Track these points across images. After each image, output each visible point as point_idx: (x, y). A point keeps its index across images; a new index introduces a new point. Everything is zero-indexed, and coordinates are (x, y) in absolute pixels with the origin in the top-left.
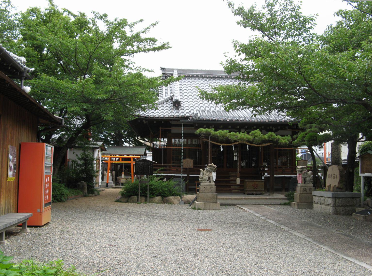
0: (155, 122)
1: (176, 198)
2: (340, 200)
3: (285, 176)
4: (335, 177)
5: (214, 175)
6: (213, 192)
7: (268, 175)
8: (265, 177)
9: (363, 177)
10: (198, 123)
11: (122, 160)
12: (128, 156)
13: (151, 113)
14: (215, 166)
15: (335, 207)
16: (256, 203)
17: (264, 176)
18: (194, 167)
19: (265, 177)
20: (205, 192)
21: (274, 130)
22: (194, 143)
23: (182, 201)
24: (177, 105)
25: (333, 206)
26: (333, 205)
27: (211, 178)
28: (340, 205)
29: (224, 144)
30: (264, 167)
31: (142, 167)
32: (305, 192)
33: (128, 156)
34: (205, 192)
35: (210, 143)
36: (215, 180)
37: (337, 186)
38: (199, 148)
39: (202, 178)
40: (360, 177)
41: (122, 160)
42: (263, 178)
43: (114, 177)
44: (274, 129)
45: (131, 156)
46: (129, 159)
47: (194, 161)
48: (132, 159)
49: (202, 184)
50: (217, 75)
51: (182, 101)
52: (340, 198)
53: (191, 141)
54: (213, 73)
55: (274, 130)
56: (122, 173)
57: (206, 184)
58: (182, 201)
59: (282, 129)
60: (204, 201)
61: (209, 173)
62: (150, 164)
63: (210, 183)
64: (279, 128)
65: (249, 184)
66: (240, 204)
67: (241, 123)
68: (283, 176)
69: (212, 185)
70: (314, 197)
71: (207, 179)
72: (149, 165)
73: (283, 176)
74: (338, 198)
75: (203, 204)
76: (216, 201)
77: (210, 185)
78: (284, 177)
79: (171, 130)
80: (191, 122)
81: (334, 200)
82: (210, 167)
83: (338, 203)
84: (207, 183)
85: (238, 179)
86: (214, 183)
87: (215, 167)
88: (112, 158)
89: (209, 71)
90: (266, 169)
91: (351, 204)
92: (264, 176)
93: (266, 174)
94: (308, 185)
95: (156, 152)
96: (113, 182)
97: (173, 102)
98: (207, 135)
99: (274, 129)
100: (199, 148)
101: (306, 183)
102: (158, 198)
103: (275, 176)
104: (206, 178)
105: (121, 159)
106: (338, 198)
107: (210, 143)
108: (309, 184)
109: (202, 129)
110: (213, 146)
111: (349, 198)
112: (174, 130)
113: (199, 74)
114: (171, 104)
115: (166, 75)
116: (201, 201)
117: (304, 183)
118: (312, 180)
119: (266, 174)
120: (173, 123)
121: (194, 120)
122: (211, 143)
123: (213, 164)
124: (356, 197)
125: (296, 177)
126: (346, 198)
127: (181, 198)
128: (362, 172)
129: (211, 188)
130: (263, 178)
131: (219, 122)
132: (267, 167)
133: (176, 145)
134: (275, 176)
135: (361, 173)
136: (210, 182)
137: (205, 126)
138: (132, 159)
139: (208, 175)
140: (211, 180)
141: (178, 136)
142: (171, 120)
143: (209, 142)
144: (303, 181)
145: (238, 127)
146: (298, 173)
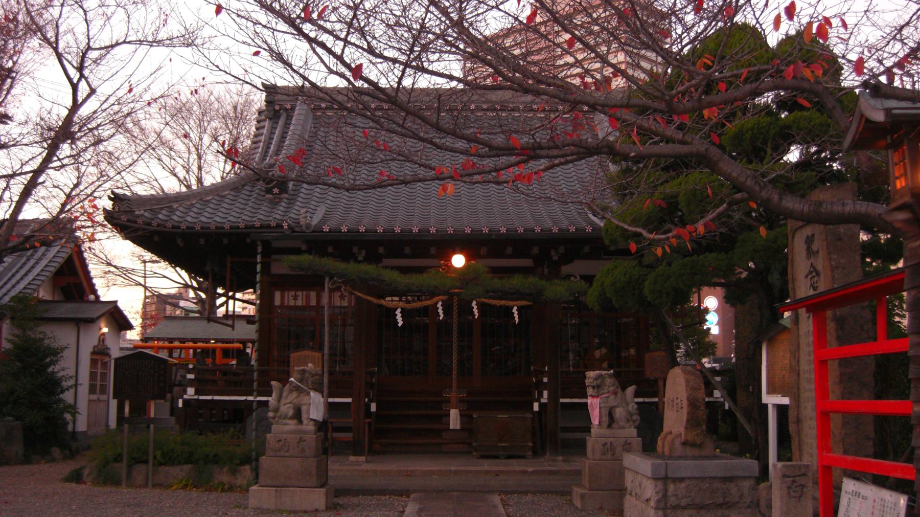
0: (225, 241)
2: (683, 485)
8: (186, 402)
9: (774, 405)
15: (665, 509)
17: (185, 397)
19: (186, 402)
22: (292, 303)
25: (657, 509)
26: (658, 501)
27: (304, 408)
28: (683, 503)
30: (540, 373)
32: (609, 456)
34: (282, 453)
39: (276, 410)
40: (766, 406)
52: (682, 480)
53: (282, 297)
57: (287, 428)
61: (295, 394)
63: (299, 427)
69: (305, 432)
70: (627, 472)
71: (291, 413)
73: (574, 400)
74: (675, 480)
78: (212, 400)
81: (660, 485)
83: (676, 495)
84: (292, 425)
85: (454, 414)
86: (311, 427)
90: (191, 376)
91: (720, 500)
92: (185, 397)
93: (191, 391)
94: (620, 432)
96: (173, 419)
101: (614, 425)
102: (180, 472)
103: (562, 400)
104: (287, 409)
106: (675, 480)
108: (624, 428)
111: (714, 478)
117: (609, 426)
118: (635, 417)
119: (191, 391)
124: (740, 477)
125: (587, 403)
126: (703, 479)
129: (301, 440)
134: (562, 400)
135: (769, 392)
140: (304, 416)
144: (606, 419)
146: (590, 391)
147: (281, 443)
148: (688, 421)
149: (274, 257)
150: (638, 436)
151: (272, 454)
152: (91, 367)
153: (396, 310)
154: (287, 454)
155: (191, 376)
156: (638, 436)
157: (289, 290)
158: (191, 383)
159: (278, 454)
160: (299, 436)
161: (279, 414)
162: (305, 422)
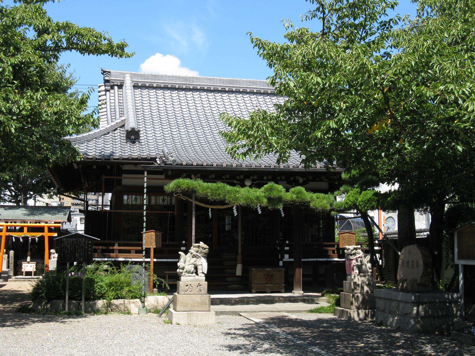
0: (94, 167)
1: (134, 303)
3: (319, 260)
4: (416, 265)
5: (203, 264)
6: (203, 292)
7: (290, 258)
8: (284, 262)
10: (172, 170)
11: (28, 231)
12: (38, 224)
13: (337, 232)
14: (206, 246)
16: (274, 310)
17: (284, 260)
18: (162, 245)
19: (284, 262)
20: (188, 292)
21: (301, 182)
22: (161, 203)
23: (144, 307)
24: (133, 137)
29: (213, 207)
30: (282, 246)
31: (67, 245)
33: (38, 224)
35: (194, 205)
36: (206, 273)
37: (419, 281)
38: (172, 212)
41: (28, 231)
42: (281, 263)
43: (12, 261)
44: (301, 180)
45: (42, 224)
46: (41, 229)
47: (162, 235)
48: (46, 229)
49: (182, 278)
50: (199, 85)
51: (141, 129)
54: (193, 82)
55: (301, 182)
56: (27, 253)
58: (144, 307)
59: (314, 180)
60: (188, 309)
61: (195, 259)
62: (88, 242)
64: (310, 178)
65: (257, 274)
66: (246, 312)
67: (247, 170)
68: (315, 260)
69: (200, 280)
70: (377, 300)
72: (85, 243)
73: (315, 260)
75: (186, 315)
76: (208, 309)
77: (196, 280)
78: (317, 261)
79: (121, 180)
80: (159, 167)
82: (197, 249)
87: (205, 249)
88: (9, 228)
89: (156, 76)
90: (287, 248)
92: (284, 260)
93: (287, 256)
95: (91, 218)
97: (127, 131)
98: (190, 193)
99: (301, 180)
100: (172, 212)
103: (303, 260)
105: (26, 229)
107: (194, 205)
109: (181, 180)
110: (198, 207)
112: (127, 180)
113: (169, 83)
114: (122, 135)
115: (112, 84)
116: (183, 309)
119: (287, 256)
120: (126, 167)
121: (166, 164)
122: (196, 204)
123: (202, 244)
127: (143, 302)
128: (460, 257)
130: (281, 263)
131: (210, 169)
132: (287, 245)
133: (128, 207)
136: (197, 274)
137: (185, 175)
138: (46, 229)
139: (193, 263)
140: (199, 271)
141: (138, 190)
142: (123, 164)
143: (192, 203)
145: (242, 177)
147: (187, 287)
148: (423, 273)
149: (124, 175)
150: (206, 281)
151: (183, 293)
152: (162, 241)
153: (233, 207)
154: (191, 293)
155: (287, 248)
156: (206, 281)
157: (160, 195)
158: (287, 252)
159: (186, 293)
160: (198, 283)
161: (185, 270)
162: (200, 274)
